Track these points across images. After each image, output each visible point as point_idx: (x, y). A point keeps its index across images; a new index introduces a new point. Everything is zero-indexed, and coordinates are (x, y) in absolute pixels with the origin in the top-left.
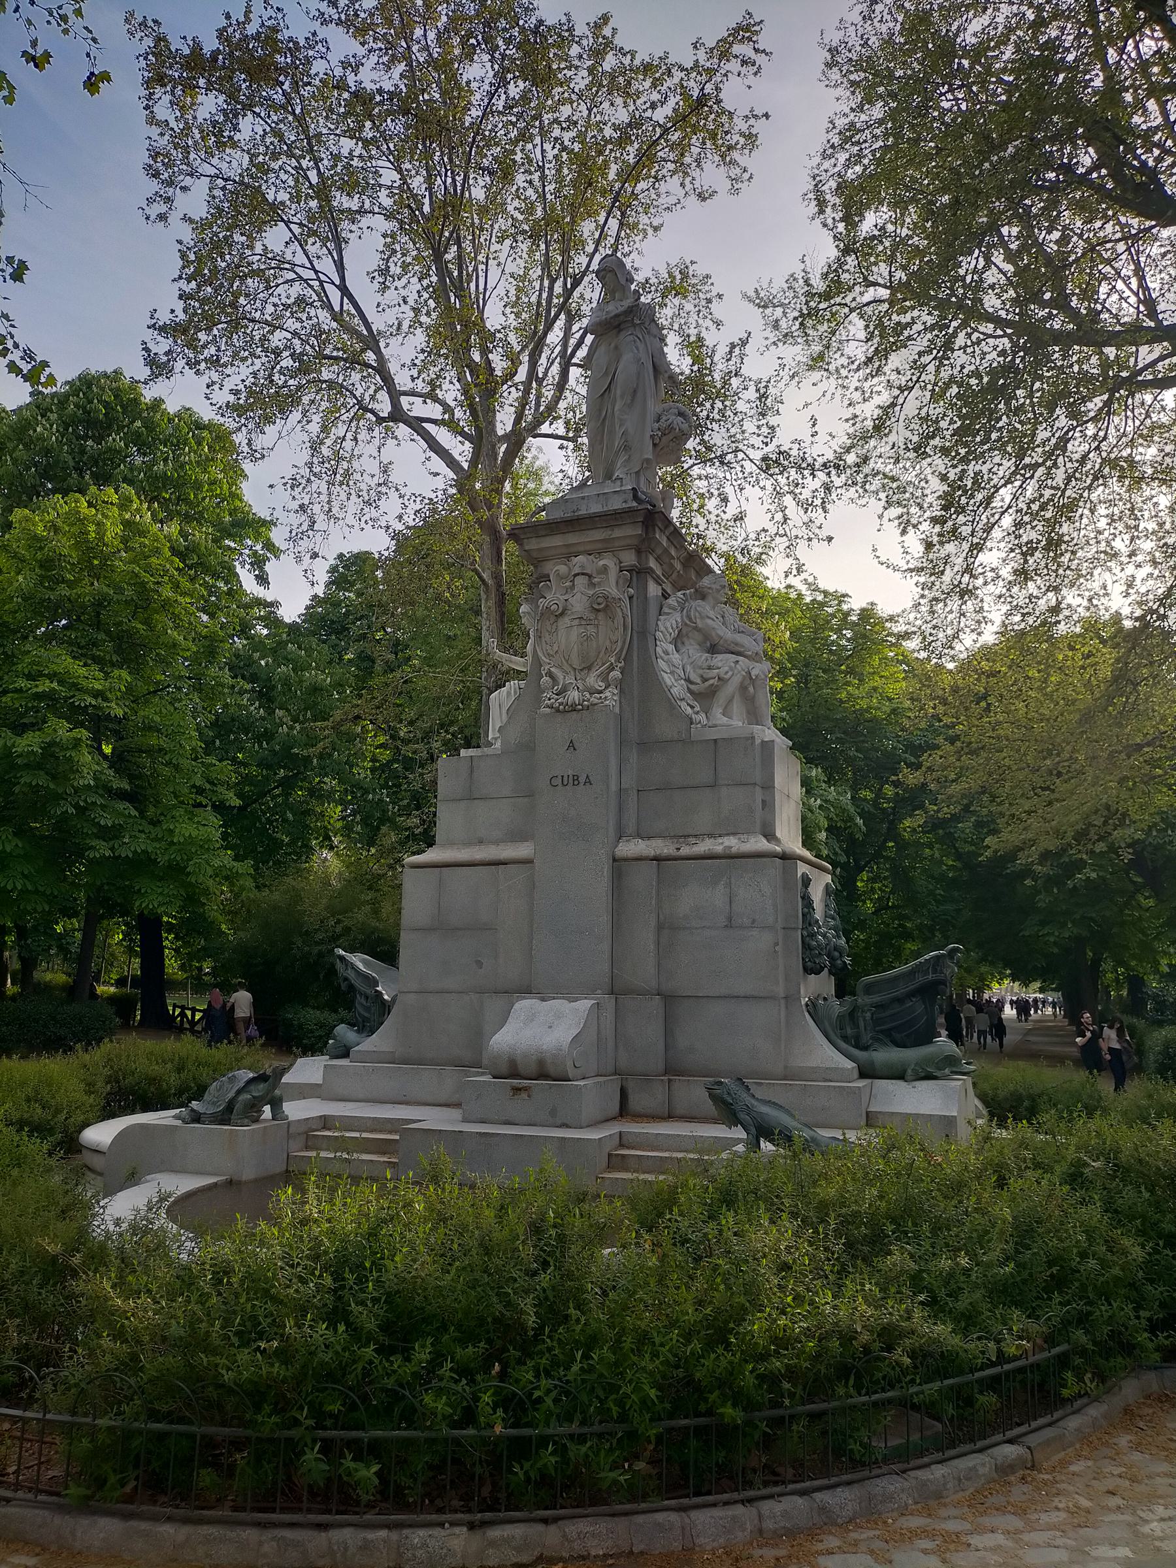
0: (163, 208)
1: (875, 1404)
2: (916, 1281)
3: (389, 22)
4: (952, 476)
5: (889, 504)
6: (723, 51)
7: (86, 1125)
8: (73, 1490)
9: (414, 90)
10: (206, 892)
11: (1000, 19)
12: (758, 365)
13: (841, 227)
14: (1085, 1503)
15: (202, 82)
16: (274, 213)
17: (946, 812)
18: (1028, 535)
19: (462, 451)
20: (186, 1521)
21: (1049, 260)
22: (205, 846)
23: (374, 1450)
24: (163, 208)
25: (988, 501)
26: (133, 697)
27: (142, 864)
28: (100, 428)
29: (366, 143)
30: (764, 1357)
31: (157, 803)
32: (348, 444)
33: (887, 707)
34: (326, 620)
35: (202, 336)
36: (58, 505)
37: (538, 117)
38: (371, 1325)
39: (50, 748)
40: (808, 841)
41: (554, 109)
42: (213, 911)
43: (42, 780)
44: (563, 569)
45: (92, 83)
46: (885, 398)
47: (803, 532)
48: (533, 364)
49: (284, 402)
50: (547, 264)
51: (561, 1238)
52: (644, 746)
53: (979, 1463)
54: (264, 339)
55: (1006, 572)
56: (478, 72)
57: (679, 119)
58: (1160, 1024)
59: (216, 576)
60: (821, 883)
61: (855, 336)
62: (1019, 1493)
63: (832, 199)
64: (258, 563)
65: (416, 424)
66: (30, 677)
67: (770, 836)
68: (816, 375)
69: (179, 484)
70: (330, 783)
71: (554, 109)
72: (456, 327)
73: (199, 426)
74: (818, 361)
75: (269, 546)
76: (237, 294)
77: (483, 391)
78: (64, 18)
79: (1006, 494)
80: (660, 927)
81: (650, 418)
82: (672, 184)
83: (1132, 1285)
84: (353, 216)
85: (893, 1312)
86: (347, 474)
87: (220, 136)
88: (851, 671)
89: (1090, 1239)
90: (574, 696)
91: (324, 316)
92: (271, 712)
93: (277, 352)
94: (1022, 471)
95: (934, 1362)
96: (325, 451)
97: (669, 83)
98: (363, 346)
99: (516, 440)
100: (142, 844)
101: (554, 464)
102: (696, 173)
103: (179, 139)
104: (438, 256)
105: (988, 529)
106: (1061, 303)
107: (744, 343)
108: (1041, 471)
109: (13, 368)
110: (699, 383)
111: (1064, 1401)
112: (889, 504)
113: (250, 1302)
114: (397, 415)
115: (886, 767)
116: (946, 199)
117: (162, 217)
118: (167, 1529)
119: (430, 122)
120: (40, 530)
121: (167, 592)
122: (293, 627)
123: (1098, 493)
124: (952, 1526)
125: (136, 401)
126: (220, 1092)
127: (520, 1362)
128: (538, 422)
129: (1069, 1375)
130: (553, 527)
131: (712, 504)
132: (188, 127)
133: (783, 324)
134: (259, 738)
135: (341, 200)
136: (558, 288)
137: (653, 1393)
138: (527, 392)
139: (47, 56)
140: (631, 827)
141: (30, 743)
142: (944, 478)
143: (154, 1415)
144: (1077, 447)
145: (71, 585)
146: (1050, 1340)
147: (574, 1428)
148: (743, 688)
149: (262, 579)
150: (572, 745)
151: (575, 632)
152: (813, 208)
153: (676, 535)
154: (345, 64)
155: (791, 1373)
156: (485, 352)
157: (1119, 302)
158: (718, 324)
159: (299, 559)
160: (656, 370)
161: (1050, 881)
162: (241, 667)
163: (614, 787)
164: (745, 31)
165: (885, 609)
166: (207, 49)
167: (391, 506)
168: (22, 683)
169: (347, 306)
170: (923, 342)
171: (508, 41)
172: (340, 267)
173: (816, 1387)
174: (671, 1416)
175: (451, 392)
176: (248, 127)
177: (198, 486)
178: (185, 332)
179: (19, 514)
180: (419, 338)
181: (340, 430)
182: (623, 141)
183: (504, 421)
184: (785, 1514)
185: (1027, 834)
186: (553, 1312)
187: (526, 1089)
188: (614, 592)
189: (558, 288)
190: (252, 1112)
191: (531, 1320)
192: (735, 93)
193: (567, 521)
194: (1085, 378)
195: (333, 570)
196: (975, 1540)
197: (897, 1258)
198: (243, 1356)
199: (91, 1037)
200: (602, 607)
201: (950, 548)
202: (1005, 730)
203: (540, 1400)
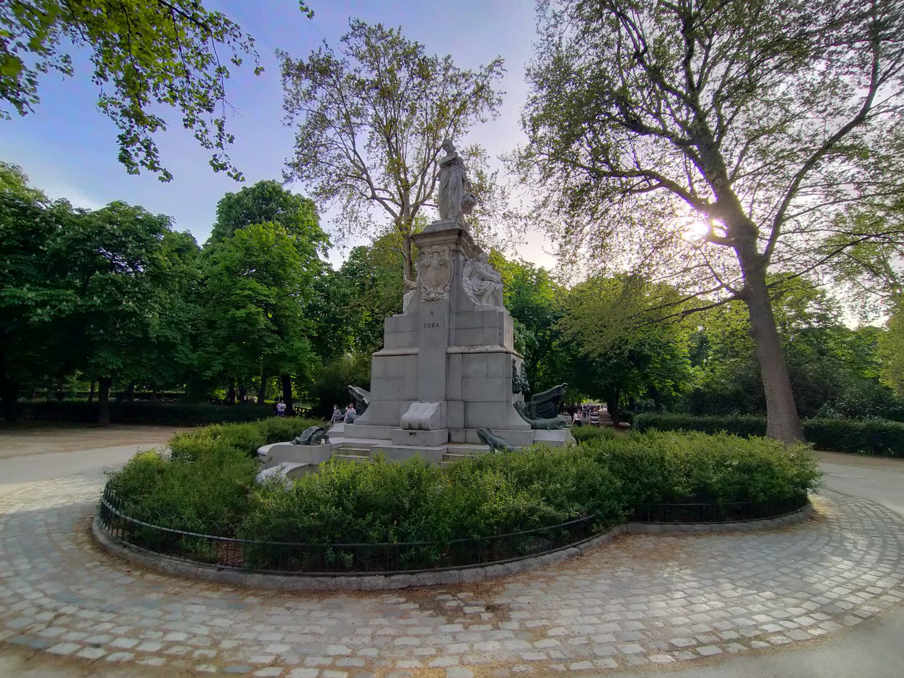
0: (289, 121)
1: (527, 534)
2: (543, 493)
3: (371, 55)
4: (569, 221)
5: (548, 231)
6: (490, 69)
7: (260, 446)
8: (246, 564)
9: (380, 81)
10: (305, 367)
11: (587, 61)
12: (501, 181)
13: (531, 133)
14: (597, 566)
15: (304, 76)
16: (330, 123)
17: (566, 339)
18: (594, 243)
19: (397, 210)
20: (285, 575)
21: (602, 146)
22: (304, 350)
23: (352, 550)
24: (289, 121)
25: (581, 231)
26: (279, 297)
27: (282, 356)
28: (268, 200)
29: (363, 99)
30: (487, 518)
31: (288, 335)
32: (356, 207)
33: (547, 303)
34: (350, 271)
35: (304, 168)
36: (251, 228)
37: (424, 91)
38: (351, 507)
39: (249, 315)
40: (517, 346)
41: (430, 89)
42: (308, 373)
43: (246, 326)
44: (429, 250)
45: (258, 71)
46: (546, 194)
47: (518, 240)
48: (423, 180)
49: (333, 192)
50: (427, 145)
51: (419, 478)
52: (458, 313)
53: (563, 554)
54: (326, 169)
55: (587, 256)
56: (403, 75)
57: (475, 93)
58: (638, 413)
59: (310, 254)
60: (520, 362)
61: (536, 173)
62: (576, 563)
63: (528, 123)
64: (325, 249)
65: (381, 200)
66: (242, 289)
67: (502, 345)
68: (522, 185)
69: (296, 221)
70: (350, 329)
71: (430, 89)
72: (396, 167)
73: (304, 201)
74: (523, 180)
75: (329, 243)
76: (316, 153)
77: (406, 187)
78: (247, 47)
79: (587, 228)
80: (463, 377)
81: (461, 197)
82: (472, 117)
83: (617, 495)
84: (359, 125)
85: (533, 503)
86: (356, 218)
87: (309, 96)
88: (535, 290)
89: (603, 480)
90: (433, 295)
91: (348, 161)
92: (329, 303)
93: (331, 174)
94: (593, 220)
95: (547, 520)
96: (348, 210)
97: (471, 80)
98: (362, 173)
99: (416, 207)
100: (282, 349)
101: (430, 214)
102: (480, 112)
103: (296, 96)
104: (389, 140)
105: (582, 240)
106: (607, 162)
107: (496, 173)
108: (599, 221)
109: (229, 174)
110: (481, 188)
111: (593, 534)
112: (548, 231)
113: (306, 501)
114: (374, 197)
115: (547, 323)
116: (567, 124)
117: (289, 124)
118: (279, 578)
119: (386, 93)
120: (245, 237)
121: (291, 260)
122: (337, 273)
123: (619, 229)
124: (551, 574)
125: (280, 191)
126: (305, 435)
127: (404, 521)
128: (424, 200)
129: (595, 525)
130: (424, 235)
131: (486, 230)
132: (298, 92)
133: (511, 167)
134: (324, 312)
135: (354, 120)
136: (432, 152)
137: (449, 530)
138: (420, 189)
139: (241, 61)
140: (453, 342)
141: (242, 313)
142: (566, 222)
143: (275, 539)
144: (612, 213)
145: (257, 256)
146: (589, 513)
147: (422, 542)
148: (493, 293)
149: (326, 256)
150: (432, 313)
151: (433, 273)
152: (522, 126)
153: (470, 239)
154: (355, 70)
155: (497, 523)
156: (405, 175)
157: (626, 163)
158: (488, 166)
159: (339, 248)
160: (463, 180)
161: (602, 364)
162: (318, 287)
163: (447, 328)
164: (498, 62)
165: (547, 269)
166: (305, 64)
167: (371, 229)
168: (238, 291)
169: (356, 158)
170: (559, 174)
171: (414, 63)
172: (354, 144)
173: (507, 529)
174: (456, 538)
175: (393, 188)
176: (321, 93)
177: (303, 222)
178: (297, 166)
179: (237, 231)
180: (382, 170)
181: (352, 203)
182: (454, 101)
183: (412, 200)
184: (495, 571)
185: (593, 347)
186: (415, 503)
187: (415, 433)
188: (447, 258)
189: (432, 152)
190: (318, 440)
191: (407, 506)
192: (494, 84)
193: (432, 233)
194: (614, 188)
195: (352, 252)
196: (559, 578)
197: (536, 485)
198: (306, 519)
199: (263, 416)
200: (443, 264)
201: (568, 247)
202: (587, 311)
203: (410, 533)
